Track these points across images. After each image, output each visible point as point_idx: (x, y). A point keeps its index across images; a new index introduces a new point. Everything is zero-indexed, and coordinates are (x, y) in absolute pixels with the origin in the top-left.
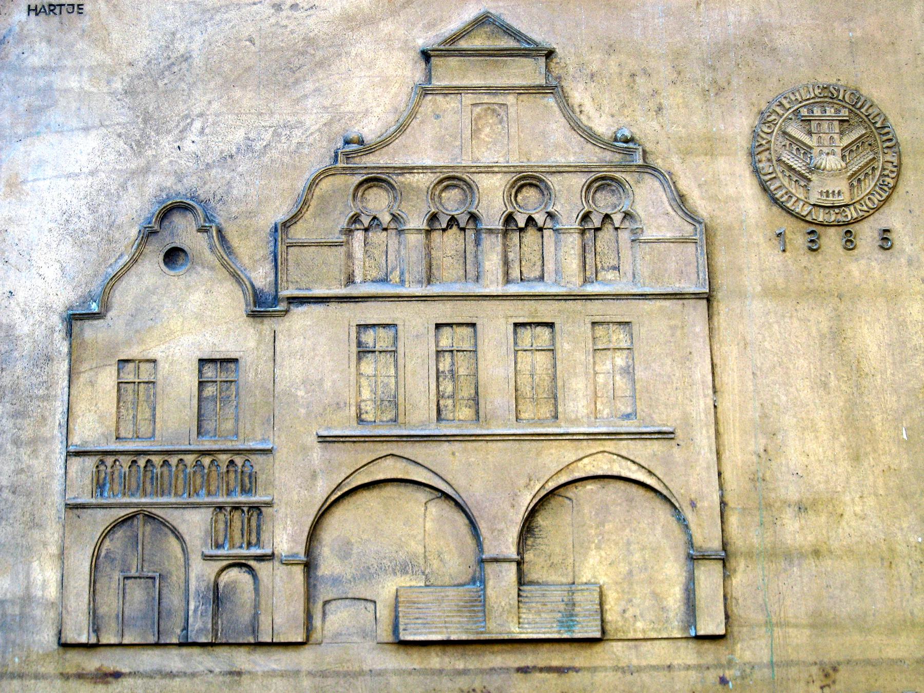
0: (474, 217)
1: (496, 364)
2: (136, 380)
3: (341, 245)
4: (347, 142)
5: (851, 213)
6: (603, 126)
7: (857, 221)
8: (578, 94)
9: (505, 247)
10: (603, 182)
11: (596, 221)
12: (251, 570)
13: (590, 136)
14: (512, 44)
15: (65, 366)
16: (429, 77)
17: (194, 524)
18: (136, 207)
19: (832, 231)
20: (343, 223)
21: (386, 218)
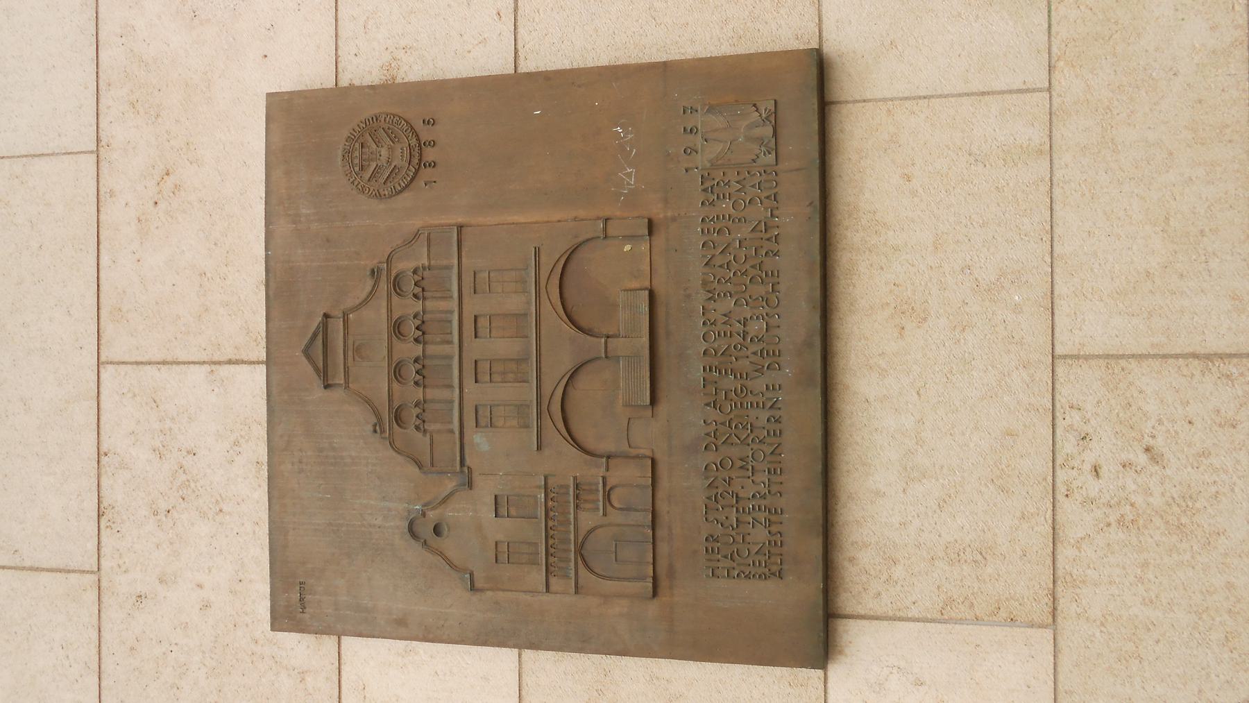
0: (416, 361)
1: (501, 346)
2: (503, 554)
3: (431, 437)
4: (375, 431)
5: (414, 142)
6: (369, 284)
7: (418, 140)
8: (350, 302)
9: (432, 343)
10: (396, 285)
11: (418, 290)
12: (611, 489)
13: (371, 294)
14: (320, 337)
15: (501, 594)
16: (340, 385)
17: (588, 520)
18: (413, 553)
19: (424, 154)
20: (420, 435)
21: (418, 410)
